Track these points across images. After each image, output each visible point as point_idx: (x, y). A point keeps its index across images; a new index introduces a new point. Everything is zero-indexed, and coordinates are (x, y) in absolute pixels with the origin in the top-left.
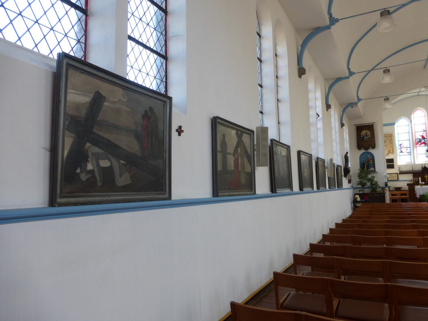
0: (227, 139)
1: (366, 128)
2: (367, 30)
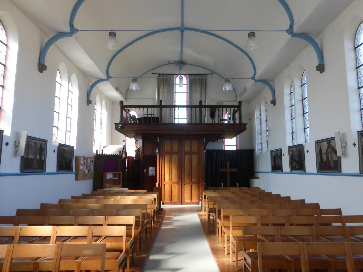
0: (322, 148)
1: (212, 114)
2: (180, 6)
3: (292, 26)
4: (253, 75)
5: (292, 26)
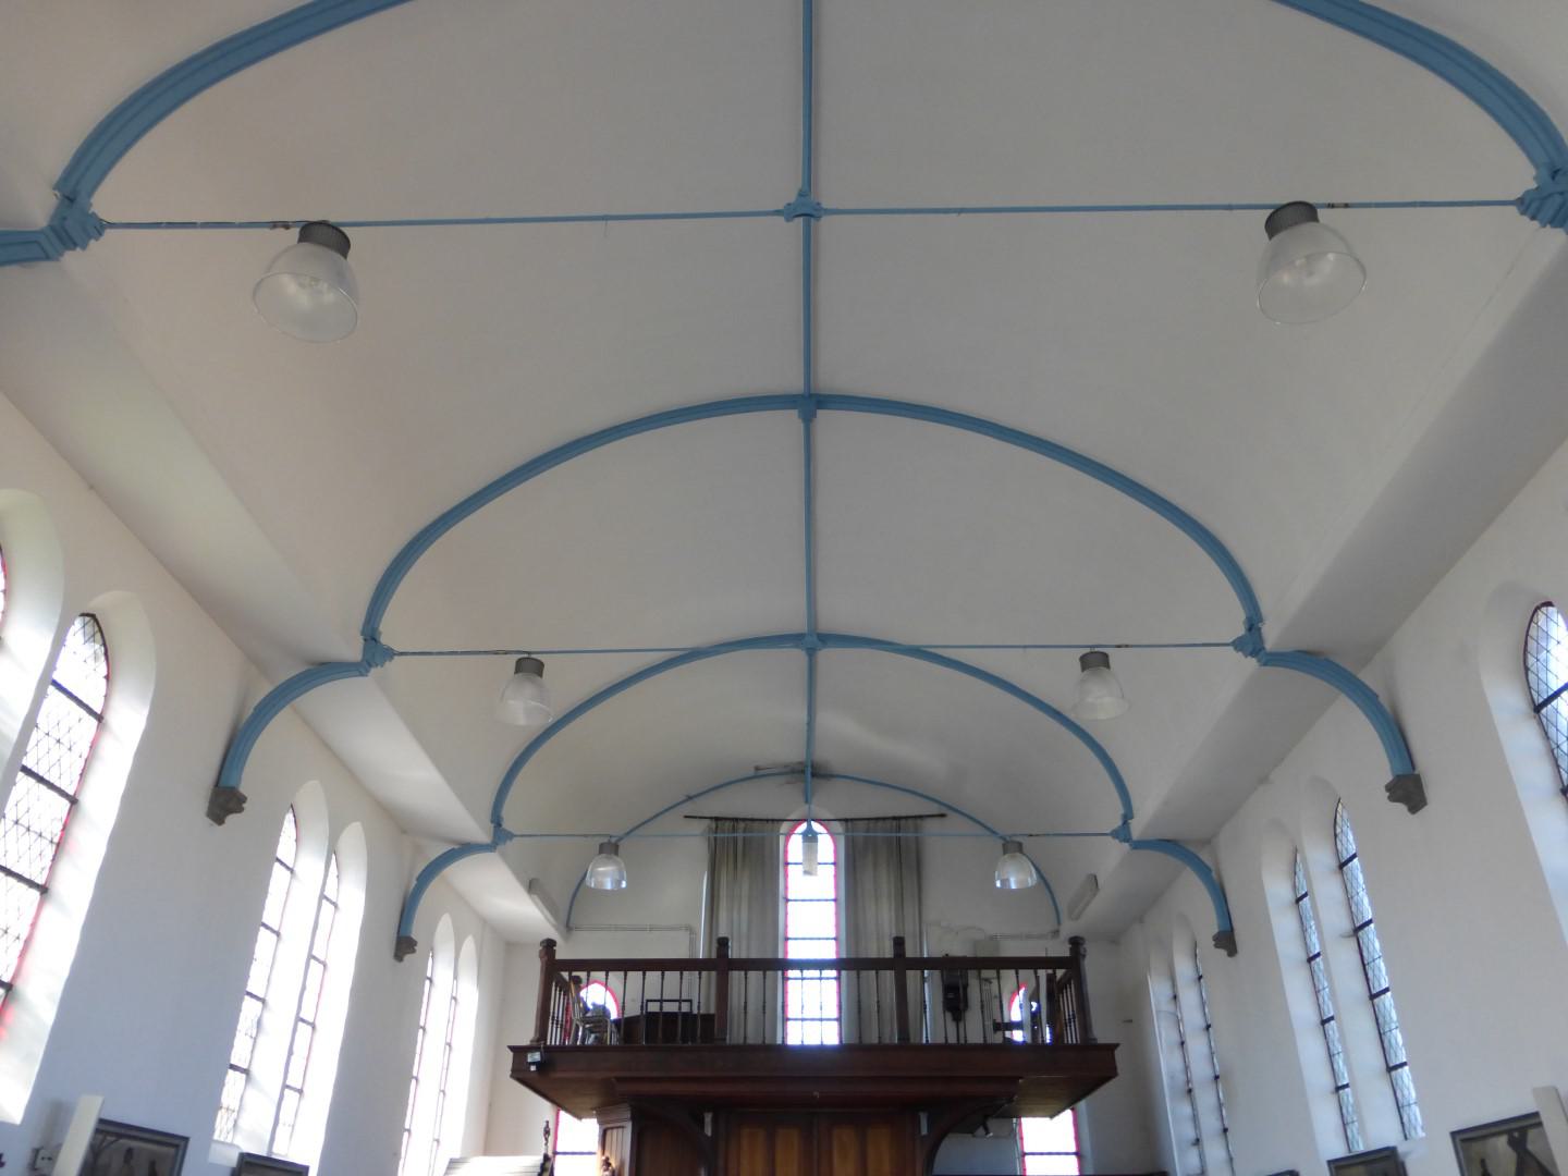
3: (1254, 624)
4: (1120, 823)
5: (1254, 624)
